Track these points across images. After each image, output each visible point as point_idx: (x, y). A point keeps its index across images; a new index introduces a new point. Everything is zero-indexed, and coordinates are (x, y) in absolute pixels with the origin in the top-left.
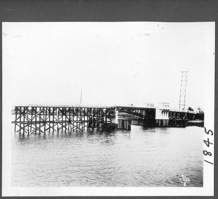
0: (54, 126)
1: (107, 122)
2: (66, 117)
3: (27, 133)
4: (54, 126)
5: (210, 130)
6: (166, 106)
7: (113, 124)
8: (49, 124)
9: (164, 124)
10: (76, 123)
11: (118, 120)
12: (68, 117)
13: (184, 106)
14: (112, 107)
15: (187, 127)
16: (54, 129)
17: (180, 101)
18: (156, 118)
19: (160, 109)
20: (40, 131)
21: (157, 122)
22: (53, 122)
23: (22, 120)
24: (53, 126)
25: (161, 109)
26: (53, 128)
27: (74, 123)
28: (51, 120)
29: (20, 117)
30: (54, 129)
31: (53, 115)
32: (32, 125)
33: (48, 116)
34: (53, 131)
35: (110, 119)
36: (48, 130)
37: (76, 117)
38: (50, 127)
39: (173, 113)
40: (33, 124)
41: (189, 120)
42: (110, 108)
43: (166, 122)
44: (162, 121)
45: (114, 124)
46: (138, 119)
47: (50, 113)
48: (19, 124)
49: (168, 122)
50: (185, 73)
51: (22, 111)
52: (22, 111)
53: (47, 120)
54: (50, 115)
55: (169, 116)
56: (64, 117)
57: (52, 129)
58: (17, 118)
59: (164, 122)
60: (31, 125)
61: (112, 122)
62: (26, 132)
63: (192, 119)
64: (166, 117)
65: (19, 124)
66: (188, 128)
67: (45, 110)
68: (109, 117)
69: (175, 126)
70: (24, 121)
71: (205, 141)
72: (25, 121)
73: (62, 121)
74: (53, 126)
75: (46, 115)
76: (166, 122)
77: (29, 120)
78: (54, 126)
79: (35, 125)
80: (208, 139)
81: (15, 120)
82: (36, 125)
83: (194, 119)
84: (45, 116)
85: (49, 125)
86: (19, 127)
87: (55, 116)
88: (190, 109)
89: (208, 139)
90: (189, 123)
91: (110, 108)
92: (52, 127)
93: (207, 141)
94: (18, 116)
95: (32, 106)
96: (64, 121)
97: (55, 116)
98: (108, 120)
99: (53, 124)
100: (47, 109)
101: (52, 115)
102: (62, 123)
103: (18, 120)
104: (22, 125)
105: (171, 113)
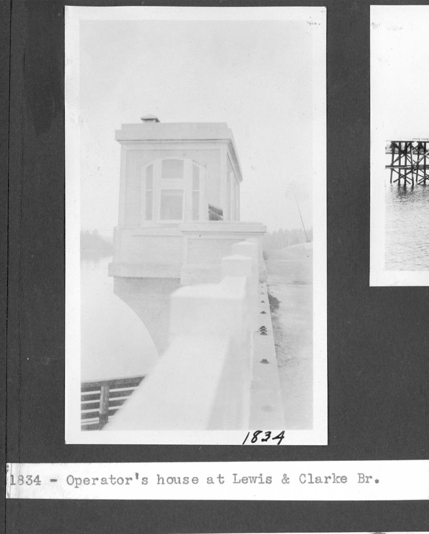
0: (406, 174)
3: (410, 183)
8: (398, 171)
23: (403, 163)
29: (399, 158)
32: (419, 171)
40: (420, 169)
48: (397, 170)
51: (403, 149)
52: (403, 149)
53: (395, 164)
58: (394, 160)
60: (417, 172)
65: (397, 170)
70: (406, 165)
77: (413, 163)
78: (398, 178)
79: (423, 170)
81: (391, 163)
94: (396, 156)
95: (418, 140)
103: (396, 164)
104: (403, 172)
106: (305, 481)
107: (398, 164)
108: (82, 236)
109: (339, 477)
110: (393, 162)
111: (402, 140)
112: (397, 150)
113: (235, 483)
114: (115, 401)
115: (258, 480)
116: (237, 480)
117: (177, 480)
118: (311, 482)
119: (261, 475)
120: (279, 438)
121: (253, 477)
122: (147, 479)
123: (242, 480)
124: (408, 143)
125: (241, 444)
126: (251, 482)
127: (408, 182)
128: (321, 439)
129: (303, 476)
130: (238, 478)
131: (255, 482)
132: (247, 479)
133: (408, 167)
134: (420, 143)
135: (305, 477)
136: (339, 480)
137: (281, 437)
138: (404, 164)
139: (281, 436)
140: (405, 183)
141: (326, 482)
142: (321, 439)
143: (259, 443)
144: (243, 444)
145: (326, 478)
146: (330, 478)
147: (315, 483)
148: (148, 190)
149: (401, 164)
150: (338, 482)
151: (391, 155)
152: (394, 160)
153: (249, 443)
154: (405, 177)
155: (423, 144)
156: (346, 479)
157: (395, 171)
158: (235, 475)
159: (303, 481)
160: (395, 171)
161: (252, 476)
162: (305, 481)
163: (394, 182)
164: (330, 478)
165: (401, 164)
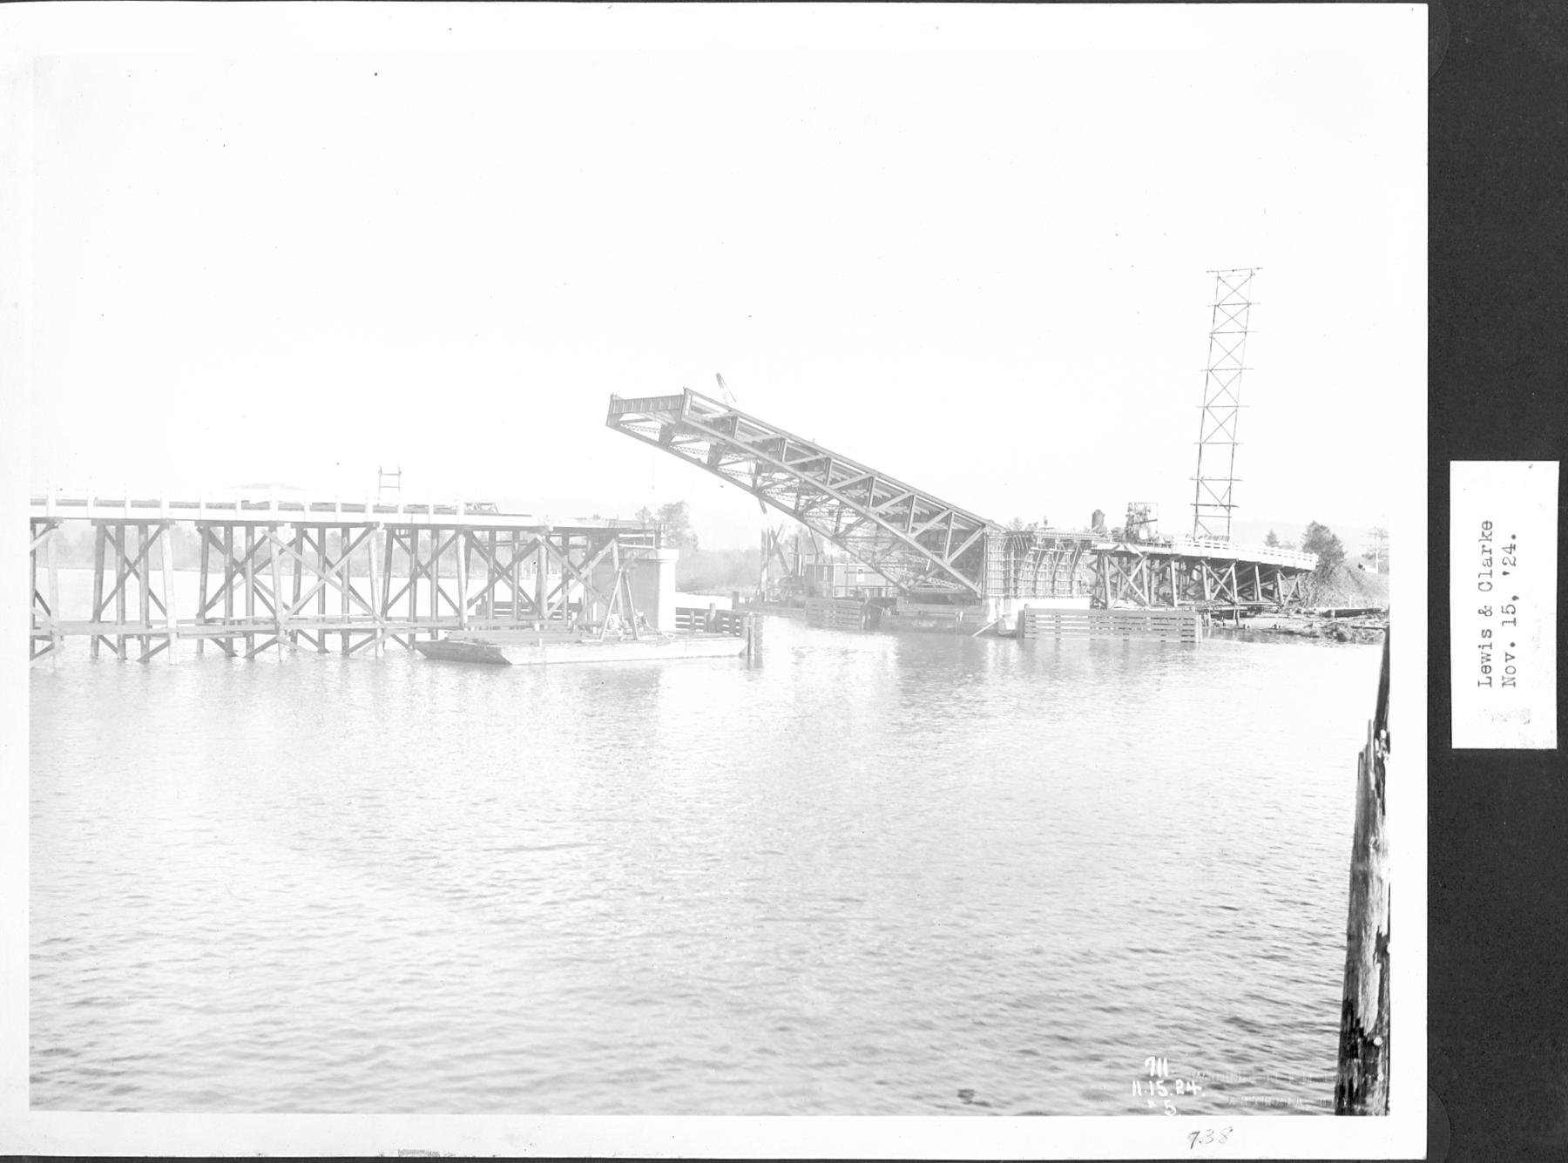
6: (1508, 568)
27: (327, 636)
50: (1235, 281)
73: (228, 620)
96: (423, 619)
101: (429, 576)
106: (1489, 583)
109: (1483, 533)
110: (205, 607)
113: (1490, 683)
114: (769, 1105)
115: (1487, 650)
116: (1488, 681)
117: (1487, 650)
118: (1491, 574)
119: (1479, 646)
121: (1483, 658)
122: (1483, 631)
123: (1486, 673)
126: (1489, 660)
128: (1462, 738)
129: (1482, 587)
130: (1484, 678)
131: (1489, 655)
132: (1486, 667)
135: (1483, 583)
136: (1487, 533)
141: (1490, 551)
142: (1462, 738)
145: (1484, 551)
146: (1484, 546)
147: (1492, 568)
150: (1491, 534)
155: (112, 529)
156: (1487, 523)
158: (1479, 684)
159: (1489, 586)
161: (1480, 660)
162: (1489, 583)
164: (1484, 546)
165: (419, 614)
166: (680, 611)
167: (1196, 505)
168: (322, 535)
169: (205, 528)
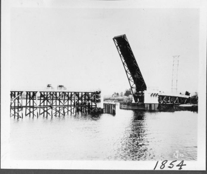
0: (33, 111)
1: (93, 107)
2: (60, 102)
3: (36, 116)
4: (33, 111)
5: (173, 165)
7: (98, 108)
9: (153, 109)
10: (59, 108)
11: (104, 104)
12: (62, 101)
13: (176, 90)
14: (97, 91)
15: (176, 112)
16: (33, 115)
17: (172, 85)
18: (145, 102)
19: (148, 93)
20: (47, 113)
21: (146, 106)
22: (33, 107)
24: (33, 111)
25: (150, 93)
26: (33, 113)
28: (32, 105)
29: (44, 102)
30: (33, 115)
31: (33, 100)
33: (54, 101)
34: (33, 116)
35: (96, 104)
36: (43, 114)
37: (70, 101)
38: (30, 112)
39: (163, 97)
40: (12, 109)
41: (180, 104)
42: (95, 92)
43: (155, 106)
44: (150, 105)
45: (100, 108)
46: (127, 103)
47: (30, 97)
49: (157, 106)
51: (70, 96)
52: (70, 96)
54: (30, 99)
55: (159, 100)
56: (70, 101)
57: (70, 112)
59: (153, 106)
61: (97, 107)
62: (30, 116)
63: (183, 103)
64: (155, 101)
65: (29, 108)
66: (177, 113)
67: (46, 95)
68: (93, 101)
69: (164, 111)
70: (60, 105)
71: (183, 161)
72: (60, 105)
74: (33, 111)
75: (53, 100)
76: (155, 106)
78: (34, 111)
80: (185, 165)
81: (39, 104)
82: (15, 110)
83: (186, 103)
84: (52, 101)
85: (30, 110)
86: (67, 110)
87: (34, 101)
88: (187, 94)
89: (185, 165)
90: (181, 107)
91: (95, 92)
92: (32, 112)
93: (183, 163)
94: (42, 101)
97: (34, 101)
98: (93, 104)
99: (33, 109)
100: (53, 93)
102: (44, 108)
104: (58, 109)
105: (161, 97)
107: (67, 104)
108: (197, 111)
111: (80, 91)
112: (28, 97)
120: (180, 166)
124: (20, 93)
125: (152, 169)
127: (30, 116)
133: (35, 107)
134: (85, 93)
137: (180, 165)
138: (70, 104)
139: (181, 165)
140: (33, 116)
143: (166, 168)
144: (154, 169)
148: (196, 105)
149: (69, 104)
151: (26, 100)
152: (41, 102)
153: (158, 168)
154: (59, 111)
157: (28, 109)
160: (28, 109)
163: (54, 114)
165: (69, 104)
166: (104, 104)
167: (172, 89)
168: (30, 94)
169: (27, 92)
